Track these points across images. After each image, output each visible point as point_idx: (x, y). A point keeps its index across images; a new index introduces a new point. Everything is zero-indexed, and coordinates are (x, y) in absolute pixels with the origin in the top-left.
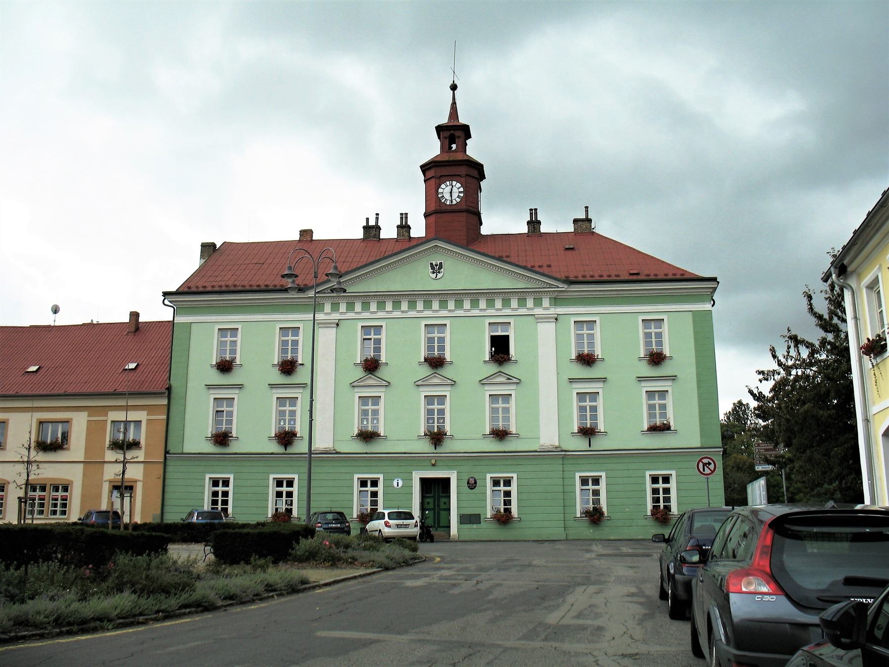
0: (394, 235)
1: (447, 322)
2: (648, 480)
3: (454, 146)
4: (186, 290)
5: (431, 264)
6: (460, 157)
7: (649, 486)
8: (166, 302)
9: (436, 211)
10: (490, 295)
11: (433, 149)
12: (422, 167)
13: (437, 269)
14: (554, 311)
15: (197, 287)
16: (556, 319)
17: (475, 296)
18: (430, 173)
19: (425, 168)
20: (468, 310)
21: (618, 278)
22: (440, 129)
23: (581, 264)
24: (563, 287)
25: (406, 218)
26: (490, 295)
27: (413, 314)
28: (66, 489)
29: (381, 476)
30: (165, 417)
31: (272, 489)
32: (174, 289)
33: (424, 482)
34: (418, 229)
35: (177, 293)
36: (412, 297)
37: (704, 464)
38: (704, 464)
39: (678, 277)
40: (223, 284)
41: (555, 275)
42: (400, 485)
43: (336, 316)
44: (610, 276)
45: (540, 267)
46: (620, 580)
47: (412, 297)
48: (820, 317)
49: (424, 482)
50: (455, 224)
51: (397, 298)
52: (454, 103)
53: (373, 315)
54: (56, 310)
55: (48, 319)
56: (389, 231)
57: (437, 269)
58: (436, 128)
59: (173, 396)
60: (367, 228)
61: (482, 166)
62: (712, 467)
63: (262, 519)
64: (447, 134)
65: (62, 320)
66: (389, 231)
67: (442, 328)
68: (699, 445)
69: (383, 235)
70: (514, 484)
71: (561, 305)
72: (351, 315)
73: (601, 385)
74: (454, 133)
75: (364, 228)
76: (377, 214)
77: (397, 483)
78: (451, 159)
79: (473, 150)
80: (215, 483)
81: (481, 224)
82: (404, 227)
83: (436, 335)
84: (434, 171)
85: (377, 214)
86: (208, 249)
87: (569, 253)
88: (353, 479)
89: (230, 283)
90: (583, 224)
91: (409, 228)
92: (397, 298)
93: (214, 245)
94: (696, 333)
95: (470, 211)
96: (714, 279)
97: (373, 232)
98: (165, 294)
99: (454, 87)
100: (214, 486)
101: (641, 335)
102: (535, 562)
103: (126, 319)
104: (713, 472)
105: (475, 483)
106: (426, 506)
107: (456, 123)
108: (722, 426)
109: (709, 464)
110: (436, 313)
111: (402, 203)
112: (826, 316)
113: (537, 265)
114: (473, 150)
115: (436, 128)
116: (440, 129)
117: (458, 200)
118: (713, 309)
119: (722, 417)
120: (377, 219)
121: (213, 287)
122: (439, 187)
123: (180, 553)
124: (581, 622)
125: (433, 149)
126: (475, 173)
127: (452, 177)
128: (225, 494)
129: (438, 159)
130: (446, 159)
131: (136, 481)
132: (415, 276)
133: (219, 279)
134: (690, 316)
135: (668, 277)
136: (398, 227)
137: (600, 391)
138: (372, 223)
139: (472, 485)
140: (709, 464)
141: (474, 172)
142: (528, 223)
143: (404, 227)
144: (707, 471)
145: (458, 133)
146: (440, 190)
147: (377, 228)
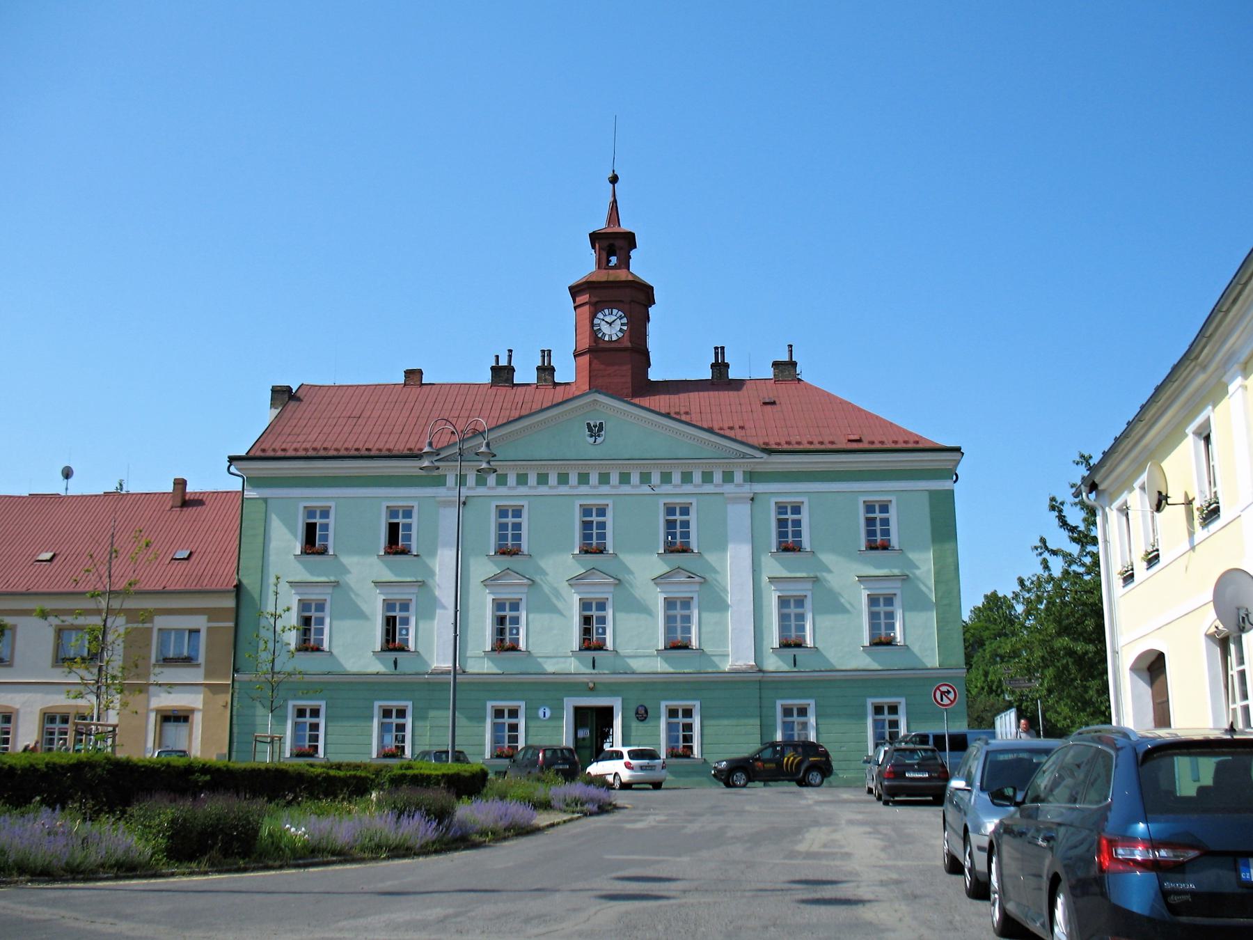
0: (533, 379)
3: (614, 260)
4: (259, 454)
5: (589, 424)
6: (622, 275)
8: (233, 469)
9: (596, 352)
11: (585, 264)
12: (571, 288)
13: (595, 431)
14: (749, 489)
15: (274, 450)
16: (752, 499)
18: (580, 300)
19: (575, 291)
20: (595, 487)
21: (833, 447)
22: (595, 237)
27: (564, 490)
28: (52, 719)
30: (232, 624)
32: (243, 453)
33: (579, 711)
34: (566, 370)
37: (942, 693)
38: (942, 693)
39: (910, 446)
40: (308, 445)
41: (750, 441)
42: (548, 715)
45: (731, 428)
46: (851, 822)
48: (1073, 529)
49: (579, 711)
50: (620, 365)
54: (67, 473)
55: (57, 486)
56: (525, 373)
57: (595, 431)
58: (591, 235)
60: (496, 370)
61: (652, 288)
62: (952, 696)
63: (365, 759)
64: (606, 243)
65: (76, 487)
66: (525, 373)
67: (877, 640)
70: (902, 710)
71: (759, 481)
72: (481, 491)
74: (614, 243)
75: (493, 368)
76: (510, 351)
78: (611, 279)
79: (641, 266)
81: (649, 365)
82: (546, 371)
85: (510, 351)
87: (769, 407)
89: (318, 445)
90: (785, 369)
91: (553, 369)
93: (289, 389)
95: (635, 350)
96: (958, 450)
97: (504, 375)
98: (232, 459)
99: (614, 180)
101: (862, 522)
102: (748, 808)
103: (170, 489)
104: (952, 702)
105: (646, 712)
107: (616, 229)
108: (966, 628)
109: (949, 692)
111: (549, 333)
112: (1082, 528)
113: (726, 426)
114: (641, 266)
115: (591, 235)
116: (595, 237)
117: (620, 335)
118: (956, 487)
119: (966, 616)
120: (510, 356)
121: (296, 450)
124: (827, 850)
125: (585, 264)
126: (641, 297)
127: (610, 304)
129: (594, 279)
130: (604, 279)
131: (192, 711)
133: (301, 438)
134: (926, 496)
136: (538, 369)
138: (503, 362)
140: (949, 692)
142: (713, 366)
143: (546, 371)
144: (946, 701)
145: (618, 243)
147: (510, 370)
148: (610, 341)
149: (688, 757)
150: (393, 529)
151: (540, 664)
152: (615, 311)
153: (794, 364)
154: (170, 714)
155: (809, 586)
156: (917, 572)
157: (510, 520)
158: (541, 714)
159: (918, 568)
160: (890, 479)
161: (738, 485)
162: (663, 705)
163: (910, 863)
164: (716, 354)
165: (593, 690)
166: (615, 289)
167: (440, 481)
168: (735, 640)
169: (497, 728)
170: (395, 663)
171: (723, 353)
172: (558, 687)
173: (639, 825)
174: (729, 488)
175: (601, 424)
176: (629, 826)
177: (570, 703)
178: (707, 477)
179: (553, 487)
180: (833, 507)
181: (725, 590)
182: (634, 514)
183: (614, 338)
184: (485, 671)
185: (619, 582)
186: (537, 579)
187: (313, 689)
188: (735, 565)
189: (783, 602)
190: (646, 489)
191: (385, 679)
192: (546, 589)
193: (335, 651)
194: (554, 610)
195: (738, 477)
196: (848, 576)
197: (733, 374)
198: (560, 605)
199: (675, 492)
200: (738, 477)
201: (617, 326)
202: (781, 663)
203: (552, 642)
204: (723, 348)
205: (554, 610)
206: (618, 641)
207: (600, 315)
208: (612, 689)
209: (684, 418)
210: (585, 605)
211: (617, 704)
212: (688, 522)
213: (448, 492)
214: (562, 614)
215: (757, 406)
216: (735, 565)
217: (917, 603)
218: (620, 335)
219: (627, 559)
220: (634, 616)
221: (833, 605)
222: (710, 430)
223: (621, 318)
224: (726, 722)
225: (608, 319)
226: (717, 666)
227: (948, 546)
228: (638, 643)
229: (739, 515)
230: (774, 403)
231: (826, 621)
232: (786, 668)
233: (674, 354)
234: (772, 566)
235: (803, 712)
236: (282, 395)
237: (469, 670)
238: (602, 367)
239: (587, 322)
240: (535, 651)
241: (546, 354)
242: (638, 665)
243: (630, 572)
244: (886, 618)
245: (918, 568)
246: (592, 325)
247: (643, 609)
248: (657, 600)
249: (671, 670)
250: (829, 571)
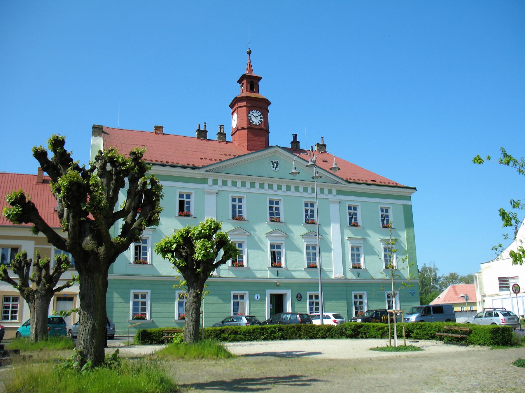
1: (245, 196)
5: (272, 161)
13: (275, 165)
16: (217, 193)
20: (276, 191)
31: (353, 300)
33: (272, 296)
42: (259, 298)
43: (216, 188)
44: (359, 180)
49: (272, 296)
57: (275, 165)
60: (199, 131)
63: (265, 320)
70: (149, 297)
72: (225, 188)
74: (251, 81)
76: (205, 123)
79: (263, 92)
85: (205, 123)
88: (130, 293)
94: (405, 216)
96: (414, 188)
99: (250, 53)
100: (142, 295)
105: (301, 297)
114: (263, 92)
117: (260, 123)
123: (123, 345)
134: (401, 208)
135: (157, 163)
137: (362, 245)
138: (202, 128)
141: (262, 105)
148: (256, 125)
149: (144, 319)
150: (181, 203)
151: (327, 274)
152: (258, 112)
153: (325, 146)
154: (68, 296)
155: (362, 242)
156: (400, 238)
157: (237, 203)
158: (256, 298)
159: (401, 237)
161: (334, 196)
164: (294, 137)
165: (277, 286)
168: (335, 266)
169: (135, 304)
171: (296, 137)
172: (257, 286)
174: (330, 197)
179: (256, 190)
180: (368, 209)
181: (331, 243)
182: (291, 205)
183: (258, 124)
184: (229, 276)
185: (250, 235)
186: (252, 232)
187: (143, 284)
188: (334, 232)
189: (352, 249)
191: (232, 280)
192: (256, 238)
193: (154, 264)
194: (260, 248)
195: (334, 192)
196: (376, 239)
197: (301, 147)
198: (262, 246)
200: (334, 192)
201: (259, 119)
202: (353, 275)
203: (295, 264)
204: (296, 135)
205: (260, 248)
206: (154, 260)
207: (251, 112)
208: (287, 286)
210: (272, 246)
211: (288, 293)
214: (263, 251)
216: (334, 232)
217: (400, 251)
218: (260, 123)
219: (292, 227)
220: (294, 252)
221: (371, 251)
223: (260, 115)
224: (333, 302)
225: (256, 115)
226: (329, 277)
227: (411, 230)
228: (295, 264)
229: (334, 209)
230: (324, 161)
231: (369, 258)
232: (355, 278)
234: (349, 233)
235: (242, 297)
237: (222, 276)
238: (253, 136)
239: (246, 115)
240: (252, 267)
241: (222, 127)
242: (259, 275)
243: (292, 232)
245: (401, 237)
246: (248, 117)
247: (298, 250)
248: (303, 245)
249: (310, 277)
250: (370, 236)
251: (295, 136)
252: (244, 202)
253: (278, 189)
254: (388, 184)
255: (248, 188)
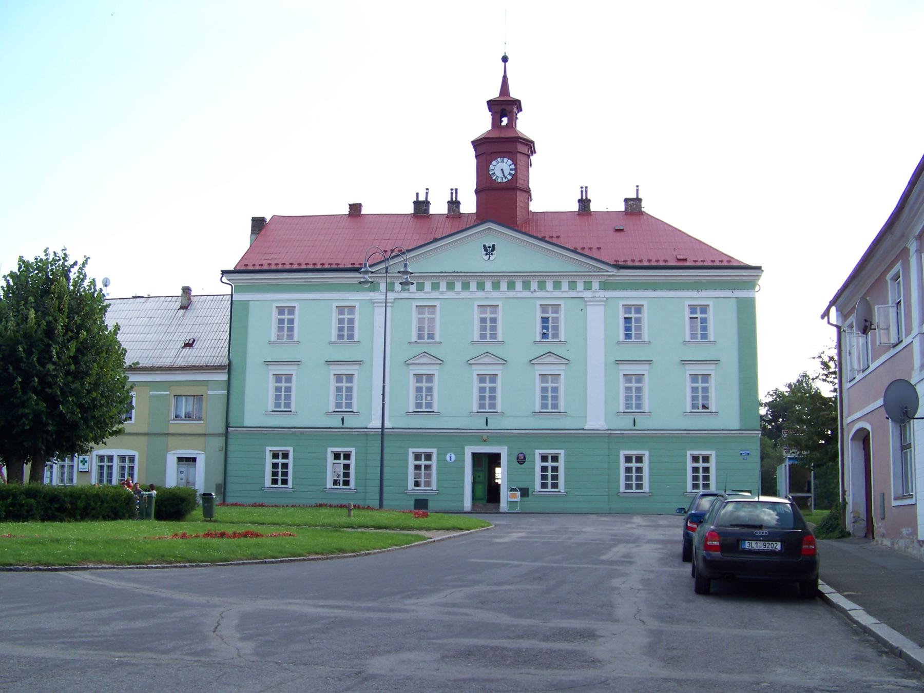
0: (444, 210)
2: (622, 459)
4: (243, 268)
5: (484, 246)
7: (690, 465)
9: (486, 187)
10: (542, 278)
11: (483, 124)
13: (489, 250)
14: (602, 294)
17: (526, 278)
22: (491, 104)
23: (630, 248)
24: (614, 272)
25: (456, 193)
26: (542, 278)
27: (465, 294)
29: (434, 451)
30: (226, 392)
32: (232, 269)
33: (475, 455)
34: (469, 205)
35: (235, 271)
36: (465, 279)
40: (280, 262)
42: (453, 459)
47: (465, 279)
50: (502, 200)
51: (451, 279)
52: (505, 78)
53: (428, 295)
56: (439, 207)
57: (489, 250)
58: (488, 102)
59: (233, 372)
60: (417, 204)
64: (499, 108)
66: (439, 207)
68: (738, 428)
69: (433, 210)
73: (646, 367)
74: (504, 107)
75: (414, 202)
77: (451, 457)
78: (502, 136)
80: (275, 455)
82: (454, 204)
83: (550, 385)
84: (486, 149)
86: (258, 224)
87: (618, 234)
91: (459, 203)
92: (451, 279)
95: (516, 189)
98: (224, 272)
99: (505, 59)
105: (525, 458)
106: (477, 479)
110: (489, 295)
111: (453, 179)
114: (525, 125)
115: (488, 102)
116: (491, 104)
122: (490, 163)
128: (285, 466)
132: (465, 254)
134: (733, 303)
138: (422, 198)
139: (521, 460)
142: (579, 201)
143: (454, 204)
146: (491, 167)
147: (427, 203)
152: (506, 160)
158: (448, 459)
160: (339, 291)
162: (538, 453)
163: (544, 564)
166: (503, 143)
167: (374, 287)
170: (343, 420)
173: (506, 540)
175: (494, 246)
176: (498, 540)
177: (469, 451)
178: (573, 286)
190: (527, 294)
195: (596, 285)
199: (550, 294)
200: (596, 285)
209: (555, 240)
211: (503, 451)
212: (557, 318)
213: (378, 296)
215: (612, 233)
222: (574, 251)
233: (550, 190)
236: (258, 224)
244: (490, 392)
251: (583, 190)
252: (711, 311)
253: (524, 288)
254: (710, 264)
255: (489, 292)
